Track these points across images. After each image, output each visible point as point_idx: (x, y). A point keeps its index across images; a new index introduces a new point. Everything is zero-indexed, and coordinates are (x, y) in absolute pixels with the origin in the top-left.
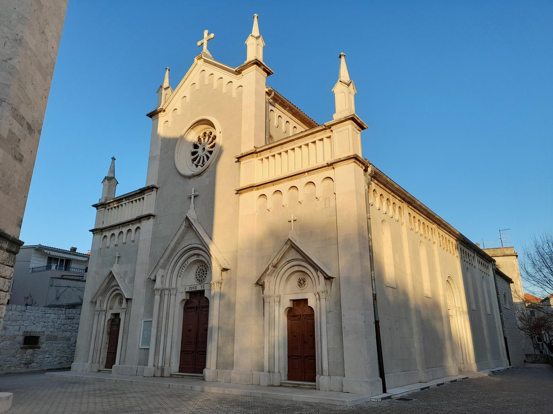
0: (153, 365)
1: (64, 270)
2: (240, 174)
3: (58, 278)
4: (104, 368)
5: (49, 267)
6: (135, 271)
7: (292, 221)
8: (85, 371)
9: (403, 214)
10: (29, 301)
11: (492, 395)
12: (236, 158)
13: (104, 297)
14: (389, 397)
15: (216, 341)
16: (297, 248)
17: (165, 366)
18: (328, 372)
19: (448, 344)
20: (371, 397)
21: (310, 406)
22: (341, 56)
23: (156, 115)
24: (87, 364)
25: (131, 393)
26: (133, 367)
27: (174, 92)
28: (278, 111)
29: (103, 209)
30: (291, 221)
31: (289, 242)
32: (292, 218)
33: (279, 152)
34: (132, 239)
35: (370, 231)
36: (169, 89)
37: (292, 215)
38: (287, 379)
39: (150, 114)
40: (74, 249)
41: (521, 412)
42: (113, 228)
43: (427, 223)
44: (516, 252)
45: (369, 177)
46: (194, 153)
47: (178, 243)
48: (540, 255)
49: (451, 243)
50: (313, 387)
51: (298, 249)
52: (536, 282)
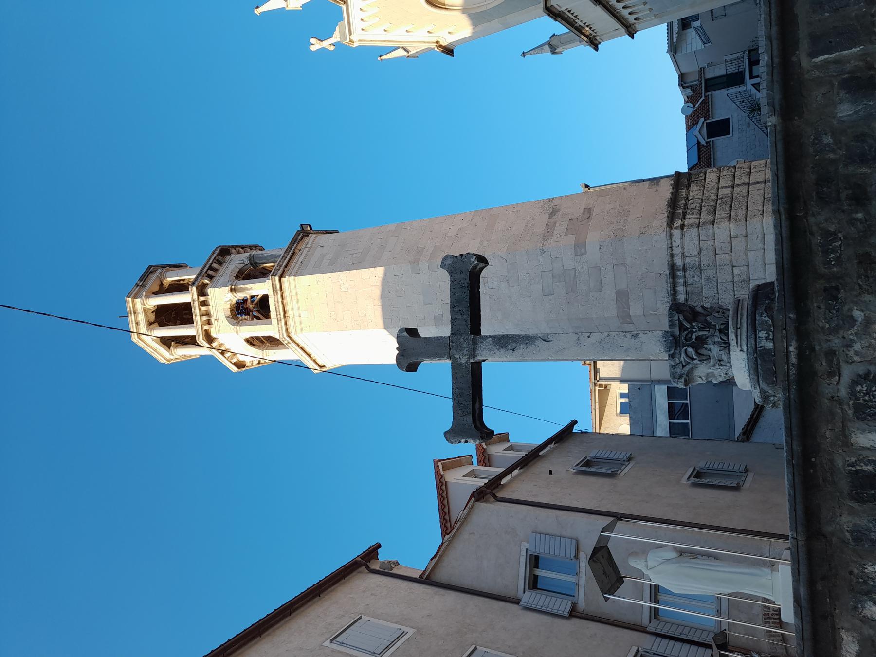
29: (597, 38)
39: (450, 55)
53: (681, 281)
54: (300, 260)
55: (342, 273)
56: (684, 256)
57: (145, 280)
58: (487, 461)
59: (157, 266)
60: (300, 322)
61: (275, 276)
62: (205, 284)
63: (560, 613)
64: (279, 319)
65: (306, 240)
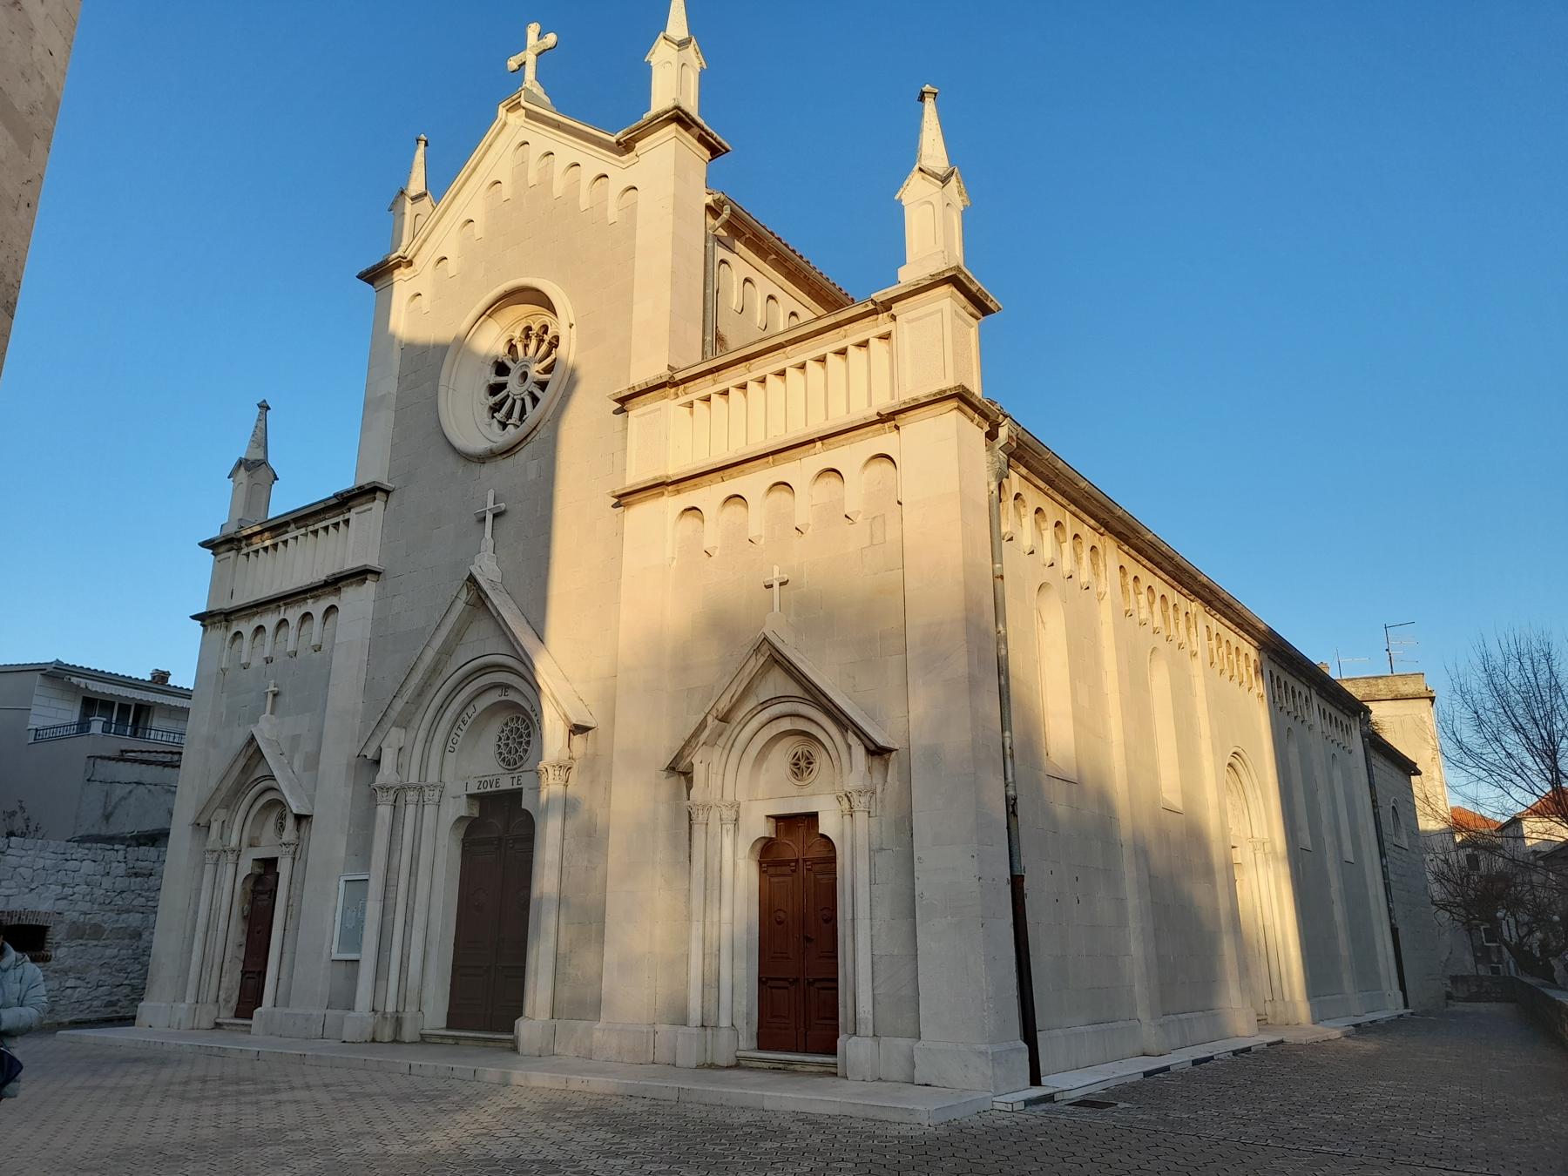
0: (369, 1006)
1: (114, 733)
2: (625, 449)
3: (109, 759)
4: (232, 1018)
5: (83, 726)
6: (321, 734)
7: (776, 585)
8: (176, 1027)
9: (1102, 568)
10: (19, 824)
11: (1348, 1091)
12: (616, 401)
13: (234, 810)
14: (1049, 1098)
15: (552, 939)
16: (789, 665)
17: (406, 1010)
18: (871, 1026)
19: (1227, 947)
20: (994, 1099)
21: (811, 1124)
22: (926, 95)
23: (387, 278)
24: (182, 1005)
25: (292, 1088)
26: (311, 1015)
27: (440, 204)
28: (741, 264)
29: (232, 554)
30: (772, 586)
31: (765, 647)
32: (776, 576)
33: (740, 381)
34: (315, 641)
35: (1000, 615)
36: (427, 199)
37: (776, 569)
38: (755, 1045)
39: (368, 272)
40: (161, 677)
41: (1426, 1139)
42: (259, 610)
43: (1174, 597)
44: (1429, 689)
45: (1003, 456)
46: (495, 389)
47: (447, 651)
48: (1495, 694)
49: (1242, 658)
50: (829, 1069)
51: (792, 668)
52: (1484, 770)
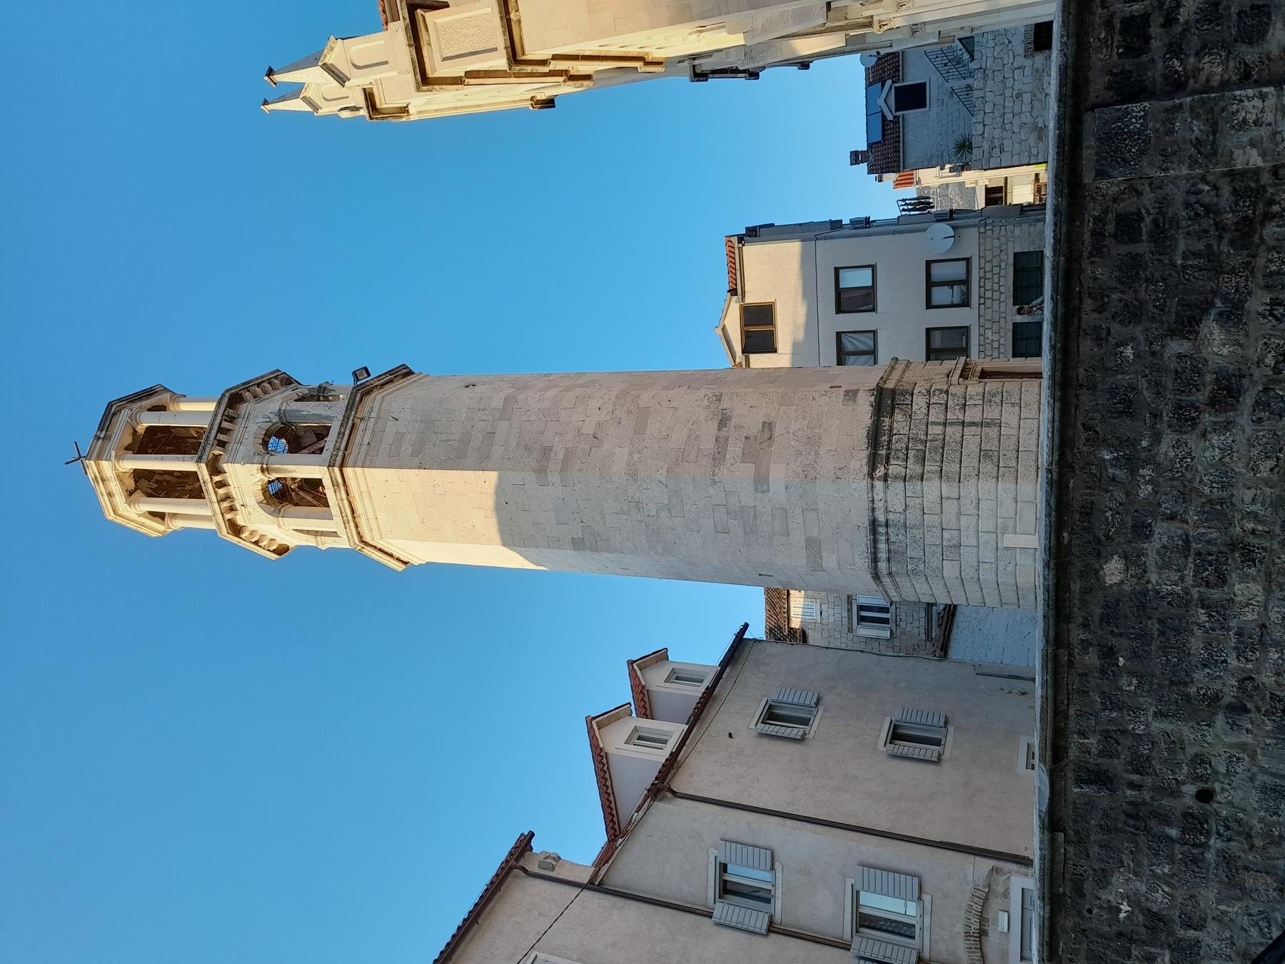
53: (883, 538)
54: (366, 440)
55: (435, 472)
56: (887, 511)
57: (108, 428)
58: (648, 713)
59: (120, 400)
60: (378, 524)
61: (334, 466)
62: (217, 456)
63: (757, 930)
64: (346, 522)
65: (368, 400)
